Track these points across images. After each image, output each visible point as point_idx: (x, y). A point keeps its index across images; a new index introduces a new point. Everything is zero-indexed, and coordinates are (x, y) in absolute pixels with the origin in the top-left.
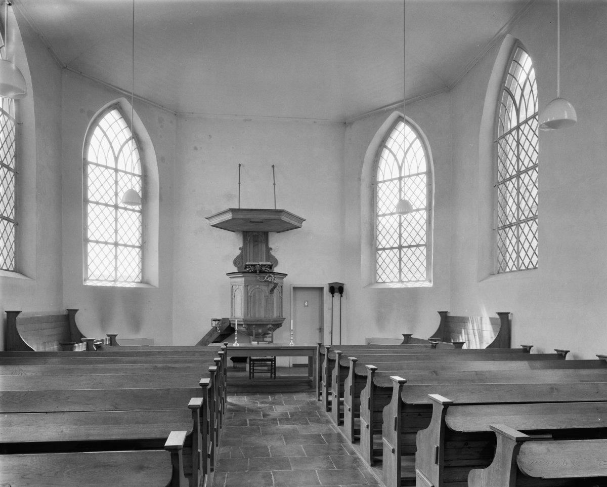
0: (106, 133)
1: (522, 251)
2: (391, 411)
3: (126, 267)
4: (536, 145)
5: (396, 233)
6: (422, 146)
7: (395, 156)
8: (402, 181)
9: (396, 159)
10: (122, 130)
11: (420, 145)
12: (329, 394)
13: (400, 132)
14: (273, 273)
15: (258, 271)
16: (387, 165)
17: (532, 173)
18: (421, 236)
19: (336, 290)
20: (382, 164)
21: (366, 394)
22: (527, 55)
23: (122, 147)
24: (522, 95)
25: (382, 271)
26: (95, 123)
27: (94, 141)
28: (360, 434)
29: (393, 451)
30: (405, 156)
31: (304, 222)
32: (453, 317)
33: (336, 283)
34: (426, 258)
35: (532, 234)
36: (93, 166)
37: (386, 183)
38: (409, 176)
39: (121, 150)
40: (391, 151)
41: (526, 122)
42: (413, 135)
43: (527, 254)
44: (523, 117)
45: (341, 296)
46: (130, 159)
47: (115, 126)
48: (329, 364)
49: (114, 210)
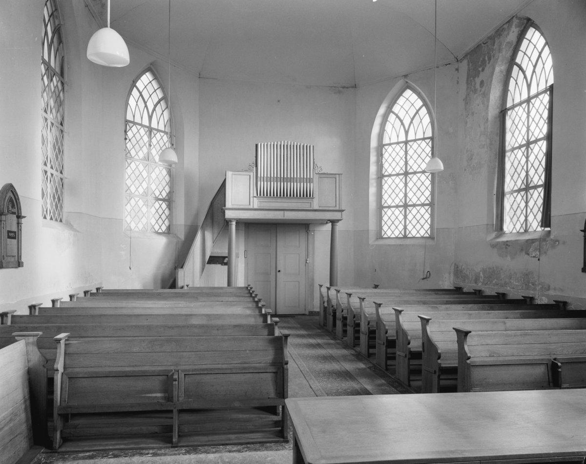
4: (542, 159)
9: (402, 124)
17: (544, 97)
18: (426, 195)
20: (388, 127)
24: (534, 71)
37: (393, 146)
38: (415, 140)
39: (154, 110)
40: (397, 116)
41: (537, 96)
42: (419, 103)
43: (530, 60)
44: (533, 91)
47: (150, 87)
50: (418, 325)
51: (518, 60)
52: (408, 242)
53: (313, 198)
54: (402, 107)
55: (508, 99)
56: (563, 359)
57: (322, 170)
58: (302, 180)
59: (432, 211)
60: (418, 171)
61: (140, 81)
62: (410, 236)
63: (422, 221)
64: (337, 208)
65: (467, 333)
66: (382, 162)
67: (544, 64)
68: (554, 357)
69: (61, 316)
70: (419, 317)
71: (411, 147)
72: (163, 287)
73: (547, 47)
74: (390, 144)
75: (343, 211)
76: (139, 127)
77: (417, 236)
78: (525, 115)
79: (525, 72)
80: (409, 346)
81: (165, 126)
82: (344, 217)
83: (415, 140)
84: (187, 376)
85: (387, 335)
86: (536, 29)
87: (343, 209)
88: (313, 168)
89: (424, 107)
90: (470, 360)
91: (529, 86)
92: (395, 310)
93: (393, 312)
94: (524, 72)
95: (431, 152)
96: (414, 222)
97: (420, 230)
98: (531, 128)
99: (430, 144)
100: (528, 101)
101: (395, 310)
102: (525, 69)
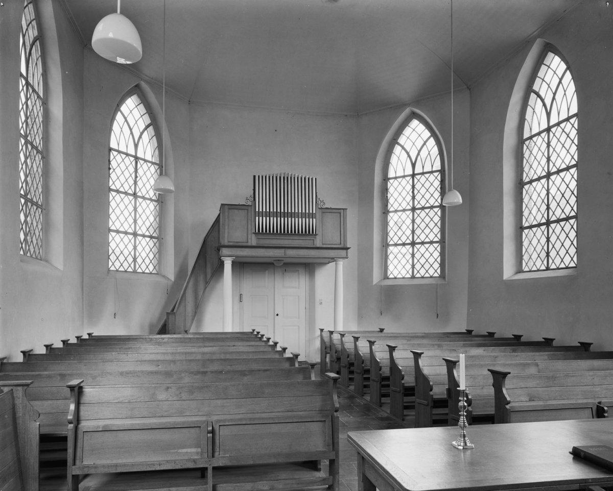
0: (127, 119)
1: (544, 196)
4: (574, 239)
5: (408, 195)
6: (436, 144)
7: (408, 153)
8: (412, 206)
9: (409, 156)
11: (435, 143)
13: (414, 130)
20: (394, 160)
23: (142, 134)
24: (554, 98)
27: (116, 127)
30: (418, 154)
35: (560, 239)
36: (115, 153)
38: (423, 174)
39: (140, 137)
40: (403, 147)
41: (558, 124)
42: (427, 134)
43: (549, 87)
50: (444, 370)
51: (536, 87)
52: (415, 282)
53: (316, 235)
54: (408, 138)
55: (525, 126)
56: (609, 402)
57: (324, 204)
58: (304, 215)
59: (443, 249)
61: (124, 105)
62: (139, 270)
63: (431, 260)
64: (342, 246)
65: (505, 375)
66: (387, 196)
67: (565, 91)
68: (598, 400)
69: (145, 338)
70: (443, 359)
71: (419, 180)
72: (151, 333)
73: (568, 71)
74: (396, 178)
75: (349, 248)
77: (426, 276)
78: (545, 145)
80: (431, 393)
81: (152, 156)
82: (349, 255)
83: (423, 174)
84: (221, 427)
85: (403, 382)
86: (556, 54)
87: (348, 246)
88: (316, 201)
89: (432, 139)
90: (509, 405)
91: (548, 115)
92: (414, 353)
93: (412, 355)
94: (543, 100)
95: (440, 186)
98: (551, 158)
99: (439, 178)
100: (548, 130)
101: (414, 353)
102: (544, 98)
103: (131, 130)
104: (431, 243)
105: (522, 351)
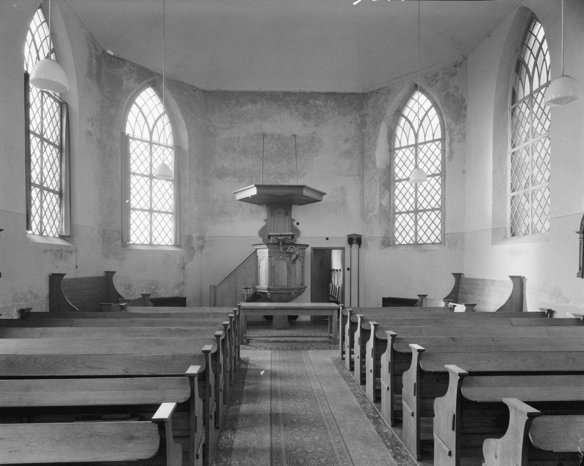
2: (410, 377)
3: (163, 232)
4: (548, 148)
6: (437, 114)
10: (156, 106)
11: (436, 113)
12: (352, 353)
14: (296, 245)
15: (281, 243)
16: (403, 132)
19: (354, 241)
20: (399, 132)
21: (386, 359)
22: (540, 25)
23: (156, 121)
24: (535, 65)
25: (403, 206)
26: (132, 101)
27: (131, 117)
28: (380, 377)
29: (413, 414)
31: (324, 196)
32: (467, 279)
33: (355, 235)
34: (441, 187)
38: (425, 143)
39: (155, 124)
40: (407, 119)
41: (538, 91)
42: (428, 104)
45: (360, 247)
46: (165, 132)
48: (352, 327)
49: (149, 215)
60: (430, 144)
62: (421, 242)
76: (138, 142)
79: (527, 65)
89: (433, 109)
96: (425, 227)
97: (435, 194)
103: (145, 118)
104: (433, 210)
105: (525, 298)
